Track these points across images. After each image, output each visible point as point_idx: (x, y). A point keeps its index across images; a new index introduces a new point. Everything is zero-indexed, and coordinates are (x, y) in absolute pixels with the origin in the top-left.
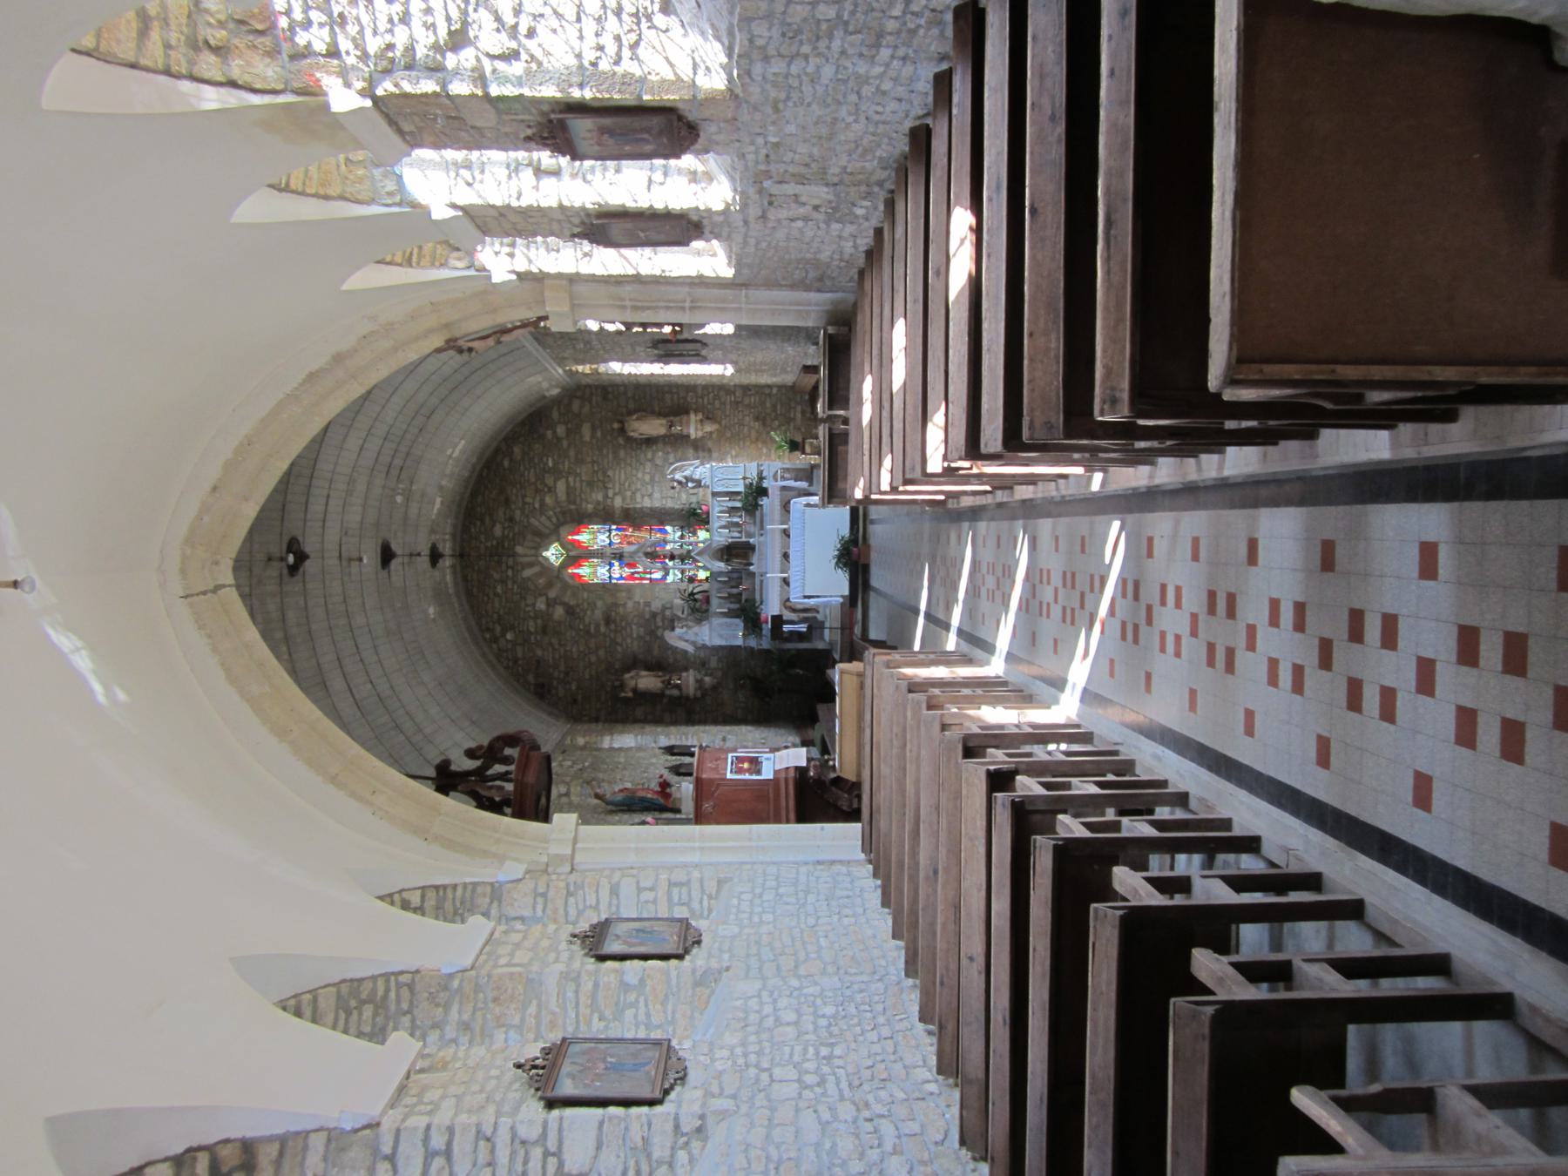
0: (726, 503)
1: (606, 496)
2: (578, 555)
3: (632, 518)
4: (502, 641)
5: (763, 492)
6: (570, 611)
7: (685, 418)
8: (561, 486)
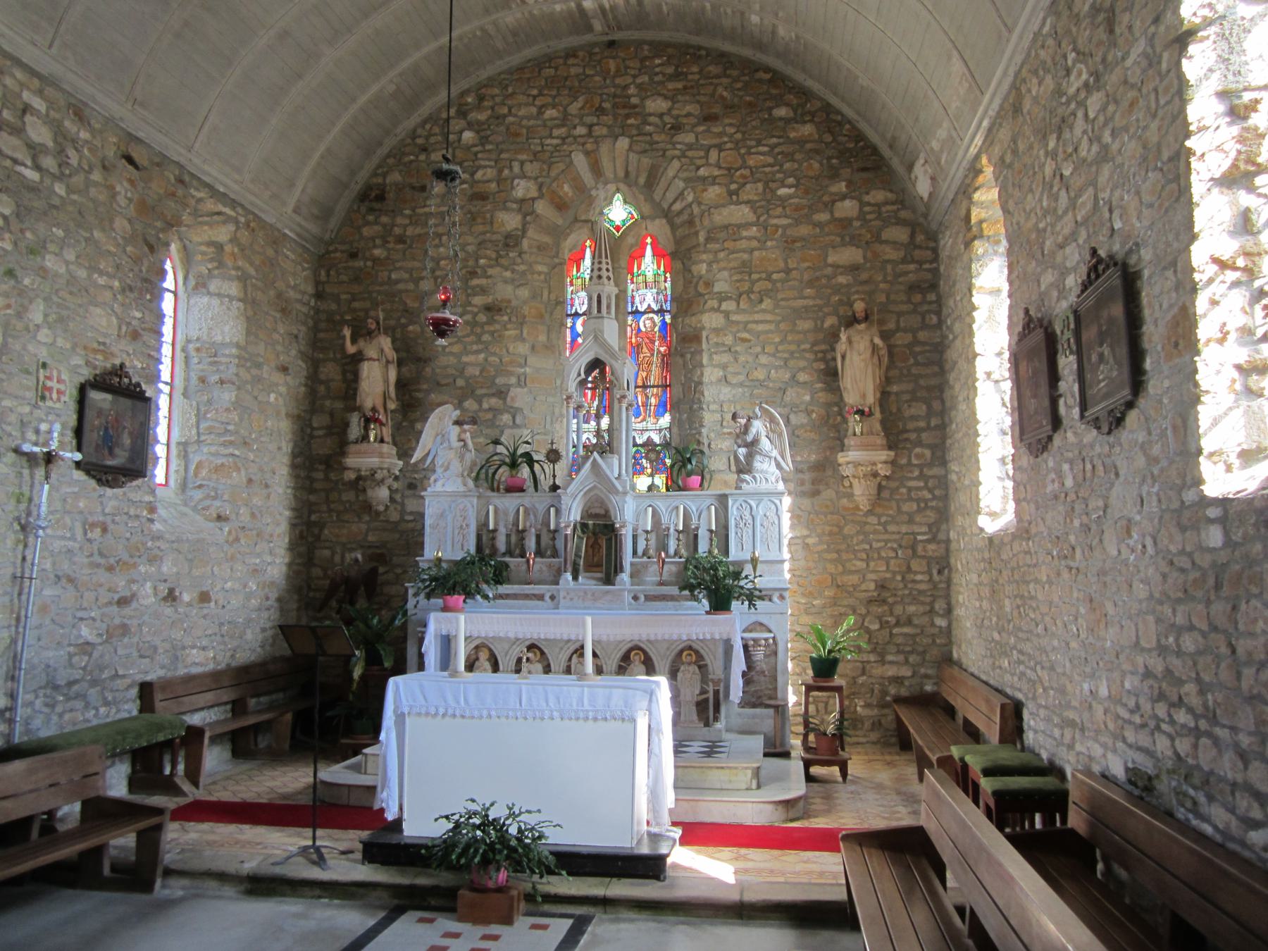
0: (707, 522)
1: (722, 298)
2: (617, 254)
3: (682, 345)
4: (462, 123)
5: (720, 603)
6: (511, 241)
7: (880, 440)
8: (741, 213)
